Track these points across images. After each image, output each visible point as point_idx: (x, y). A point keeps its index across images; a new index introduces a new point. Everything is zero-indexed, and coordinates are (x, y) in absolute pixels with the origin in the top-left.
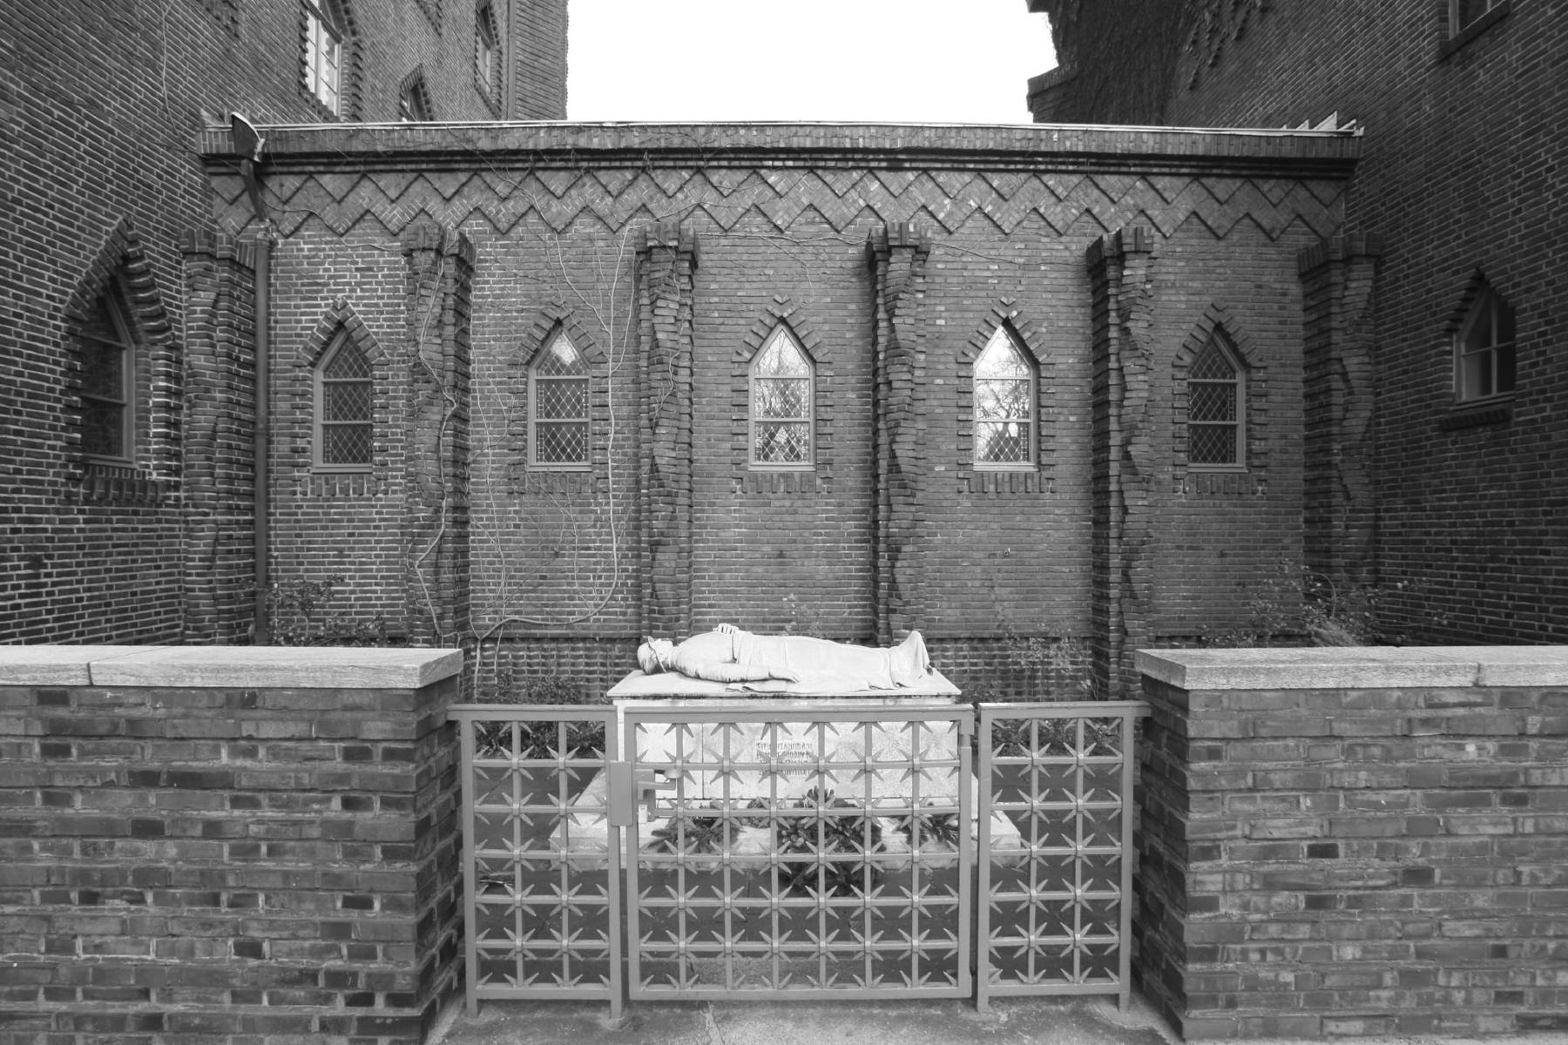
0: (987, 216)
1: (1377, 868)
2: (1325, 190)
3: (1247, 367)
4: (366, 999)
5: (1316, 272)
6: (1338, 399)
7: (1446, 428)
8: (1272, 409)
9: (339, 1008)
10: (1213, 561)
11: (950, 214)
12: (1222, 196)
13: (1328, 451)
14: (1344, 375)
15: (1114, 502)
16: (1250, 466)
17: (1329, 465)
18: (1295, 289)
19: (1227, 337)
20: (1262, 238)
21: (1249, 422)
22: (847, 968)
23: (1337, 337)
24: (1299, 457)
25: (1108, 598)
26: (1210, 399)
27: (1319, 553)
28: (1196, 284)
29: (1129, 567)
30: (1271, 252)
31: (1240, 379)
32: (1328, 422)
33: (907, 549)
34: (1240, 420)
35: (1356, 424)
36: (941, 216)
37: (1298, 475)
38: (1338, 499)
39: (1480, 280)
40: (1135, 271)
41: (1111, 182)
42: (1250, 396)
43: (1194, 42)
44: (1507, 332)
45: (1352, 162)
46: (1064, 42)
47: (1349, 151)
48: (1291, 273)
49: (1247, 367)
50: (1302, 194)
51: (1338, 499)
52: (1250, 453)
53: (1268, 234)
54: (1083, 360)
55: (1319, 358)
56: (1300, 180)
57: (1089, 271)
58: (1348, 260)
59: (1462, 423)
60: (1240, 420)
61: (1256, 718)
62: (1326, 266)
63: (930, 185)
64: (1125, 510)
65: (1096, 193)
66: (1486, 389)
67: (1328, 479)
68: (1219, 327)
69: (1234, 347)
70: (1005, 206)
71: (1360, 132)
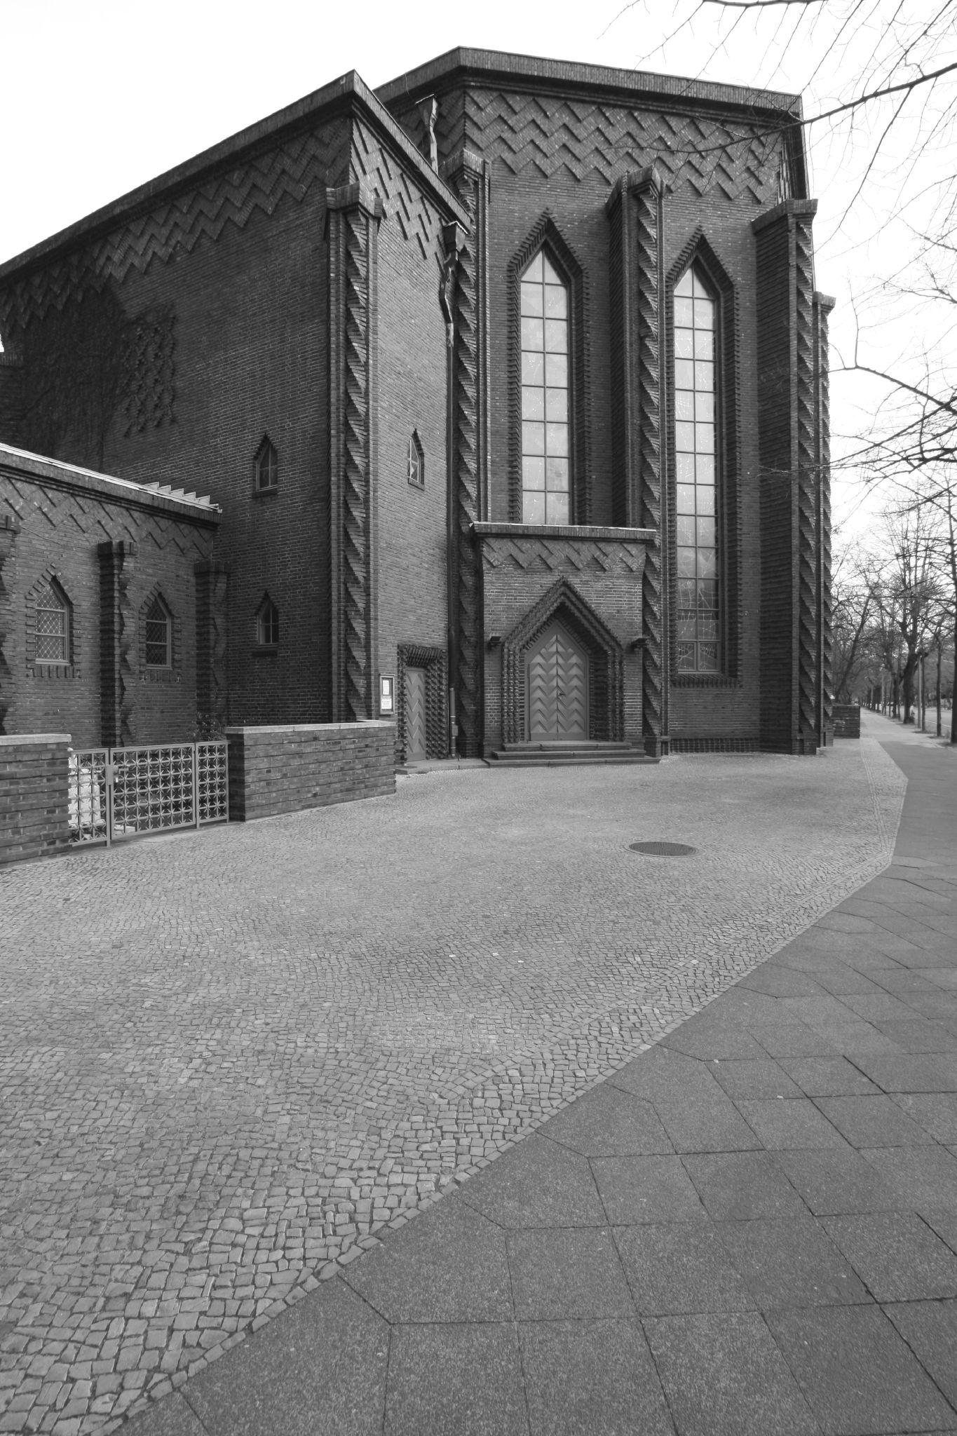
0: (44, 513)
1: (279, 775)
2: (206, 535)
3: (172, 616)
4: (53, 843)
5: (203, 573)
6: (212, 637)
7: (255, 655)
8: (181, 636)
9: (45, 847)
10: (158, 715)
11: (22, 508)
12: (163, 528)
13: (208, 662)
14: (215, 626)
15: (117, 684)
16: (174, 667)
17: (209, 668)
18: (193, 580)
19: (163, 600)
20: (178, 551)
21: (173, 644)
22: (167, 821)
23: (212, 608)
24: (194, 663)
25: (114, 735)
26: (153, 632)
27: (204, 706)
28: (150, 571)
29: (126, 718)
30: (183, 560)
31: (168, 621)
32: (208, 647)
33: (11, 710)
34: (168, 643)
35: (220, 650)
36: (17, 508)
37: (193, 672)
38: (213, 685)
39: (266, 596)
40: (129, 564)
41: (111, 508)
42: (174, 631)
43: (127, 409)
44: (276, 620)
45: (218, 524)
46: (10, 336)
47: (216, 520)
48: (191, 571)
49: (172, 616)
50: (196, 533)
51: (213, 685)
52: (173, 660)
53: (182, 550)
54: (94, 604)
55: (203, 617)
56: (196, 527)
57: (99, 556)
58: (217, 572)
59: (260, 654)
60: (168, 643)
61: (256, 741)
62: (207, 573)
63: (11, 487)
64: (123, 688)
65: (103, 513)
66: (267, 640)
67: (208, 675)
68: (160, 594)
69: (166, 605)
70: (55, 510)
71: (220, 511)
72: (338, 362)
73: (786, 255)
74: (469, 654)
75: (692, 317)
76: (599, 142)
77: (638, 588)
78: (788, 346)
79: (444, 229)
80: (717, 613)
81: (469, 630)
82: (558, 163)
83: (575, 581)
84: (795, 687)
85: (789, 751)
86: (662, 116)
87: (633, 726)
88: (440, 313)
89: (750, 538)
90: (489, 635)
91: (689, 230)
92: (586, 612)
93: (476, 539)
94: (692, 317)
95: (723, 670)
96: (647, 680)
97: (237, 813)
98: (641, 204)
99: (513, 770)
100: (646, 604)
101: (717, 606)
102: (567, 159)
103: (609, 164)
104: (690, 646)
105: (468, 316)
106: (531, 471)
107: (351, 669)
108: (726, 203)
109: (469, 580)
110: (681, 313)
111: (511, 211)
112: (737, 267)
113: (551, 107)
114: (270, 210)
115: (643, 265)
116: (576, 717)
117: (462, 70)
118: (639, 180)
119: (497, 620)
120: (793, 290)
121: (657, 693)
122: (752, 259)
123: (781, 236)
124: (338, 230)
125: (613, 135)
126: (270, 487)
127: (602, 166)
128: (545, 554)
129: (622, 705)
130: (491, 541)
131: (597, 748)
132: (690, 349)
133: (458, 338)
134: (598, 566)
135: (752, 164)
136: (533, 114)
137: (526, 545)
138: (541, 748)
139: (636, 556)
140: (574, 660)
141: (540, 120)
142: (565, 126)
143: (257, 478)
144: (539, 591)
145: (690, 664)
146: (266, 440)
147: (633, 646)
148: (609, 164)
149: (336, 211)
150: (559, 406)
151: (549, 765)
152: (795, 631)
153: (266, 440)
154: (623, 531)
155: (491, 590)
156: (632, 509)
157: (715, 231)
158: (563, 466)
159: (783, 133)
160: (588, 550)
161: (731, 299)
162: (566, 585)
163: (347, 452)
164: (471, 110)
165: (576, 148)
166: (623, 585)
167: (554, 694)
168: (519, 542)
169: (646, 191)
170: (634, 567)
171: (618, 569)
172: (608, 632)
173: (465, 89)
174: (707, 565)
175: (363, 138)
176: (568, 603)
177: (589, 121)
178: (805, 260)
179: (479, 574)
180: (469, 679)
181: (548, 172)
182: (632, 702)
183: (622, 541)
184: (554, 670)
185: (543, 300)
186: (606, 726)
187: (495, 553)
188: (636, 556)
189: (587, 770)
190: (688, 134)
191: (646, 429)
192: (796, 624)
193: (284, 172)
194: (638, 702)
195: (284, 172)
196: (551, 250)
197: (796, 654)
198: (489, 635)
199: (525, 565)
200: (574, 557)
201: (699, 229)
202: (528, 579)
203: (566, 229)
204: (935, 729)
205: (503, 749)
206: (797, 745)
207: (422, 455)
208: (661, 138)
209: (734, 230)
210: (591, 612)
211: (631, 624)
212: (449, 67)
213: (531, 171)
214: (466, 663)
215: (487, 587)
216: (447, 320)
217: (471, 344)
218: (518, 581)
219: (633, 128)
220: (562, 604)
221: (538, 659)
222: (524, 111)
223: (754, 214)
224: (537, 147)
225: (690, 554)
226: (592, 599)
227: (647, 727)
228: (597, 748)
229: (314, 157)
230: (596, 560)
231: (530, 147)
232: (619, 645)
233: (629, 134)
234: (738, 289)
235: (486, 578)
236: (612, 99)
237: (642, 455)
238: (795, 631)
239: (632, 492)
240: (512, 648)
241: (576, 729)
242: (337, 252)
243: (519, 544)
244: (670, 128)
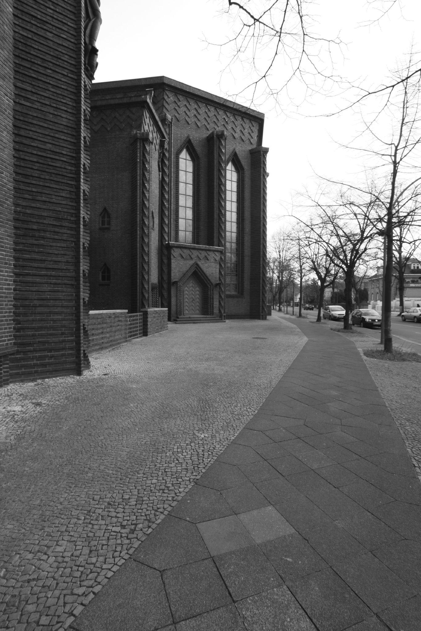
72: (140, 189)
73: (260, 163)
74: (165, 286)
75: (231, 176)
76: (206, 116)
77: (218, 266)
78: (260, 192)
79: (161, 141)
81: (165, 278)
82: (193, 120)
83: (199, 263)
84: (261, 299)
85: (259, 319)
86: (225, 112)
87: (216, 311)
88: (157, 168)
89: (247, 251)
91: (232, 149)
93: (169, 248)
94: (231, 176)
95: (239, 293)
96: (220, 296)
97: (145, 333)
98: (220, 142)
99: (183, 325)
100: (220, 272)
101: (237, 272)
102: (196, 119)
103: (209, 124)
104: (229, 285)
105: (166, 170)
106: (182, 222)
107: (144, 291)
108: (242, 143)
109: (165, 261)
110: (228, 176)
111: (179, 134)
112: (245, 163)
113: (192, 102)
114: (109, 129)
115: (220, 161)
116: (198, 308)
117: (164, 84)
118: (220, 134)
119: (176, 274)
120: (262, 175)
121: (222, 299)
122: (250, 161)
123: (258, 156)
124: (140, 146)
125: (210, 115)
126: (106, 226)
127: (206, 124)
128: (191, 254)
129: (213, 304)
130: (174, 249)
131: (206, 318)
132: (230, 187)
133: (163, 177)
134: (206, 258)
135: (250, 132)
136: (185, 103)
137: (185, 251)
138: (190, 318)
139: (218, 256)
140: (198, 289)
141: (188, 105)
142: (195, 109)
143: (101, 222)
144: (188, 266)
145: (229, 291)
146: (105, 209)
147: (217, 285)
148: (209, 124)
149: (140, 139)
150: (190, 203)
151: (194, 323)
152: (261, 281)
153: (105, 209)
154: (212, 247)
155: (174, 264)
156: (216, 240)
157: (239, 151)
158: (191, 222)
159: (259, 124)
160: (204, 254)
161: (243, 173)
162: (197, 264)
163: (143, 220)
164: (166, 97)
165: (199, 117)
166: (213, 265)
167: (191, 300)
168: (183, 250)
169: (222, 137)
170: (217, 259)
171: (212, 260)
172: (209, 280)
173: (164, 90)
174: (234, 259)
175: (146, 114)
177: (203, 109)
178: (265, 165)
179: (169, 260)
180: (165, 294)
181: (190, 123)
182: (216, 304)
183: (214, 251)
184: (190, 294)
185: (186, 164)
186: (208, 311)
187: (175, 253)
188: (218, 256)
189: (206, 324)
190: (232, 118)
191: (220, 215)
192: (261, 279)
193: (115, 117)
194: (218, 303)
195: (115, 117)
197: (261, 288)
200: (199, 255)
201: (234, 149)
202: (185, 262)
203: (195, 143)
204: (298, 314)
205: (178, 318)
206: (261, 317)
208: (224, 118)
209: (245, 151)
210: (204, 274)
211: (216, 278)
212: (159, 82)
213: (184, 122)
215: (172, 264)
216: (159, 171)
217: (167, 179)
218: (182, 262)
219: (216, 114)
221: (186, 288)
222: (183, 102)
223: (250, 148)
224: (186, 114)
225: (229, 255)
226: (205, 269)
227: (220, 311)
228: (206, 318)
229: (128, 117)
230: (206, 256)
231: (184, 113)
232: (212, 284)
233: (215, 115)
234: (245, 170)
235: (172, 261)
236: (210, 103)
237: (219, 222)
238: (261, 281)
239: (216, 235)
241: (198, 312)
242: (140, 153)
244: (227, 116)
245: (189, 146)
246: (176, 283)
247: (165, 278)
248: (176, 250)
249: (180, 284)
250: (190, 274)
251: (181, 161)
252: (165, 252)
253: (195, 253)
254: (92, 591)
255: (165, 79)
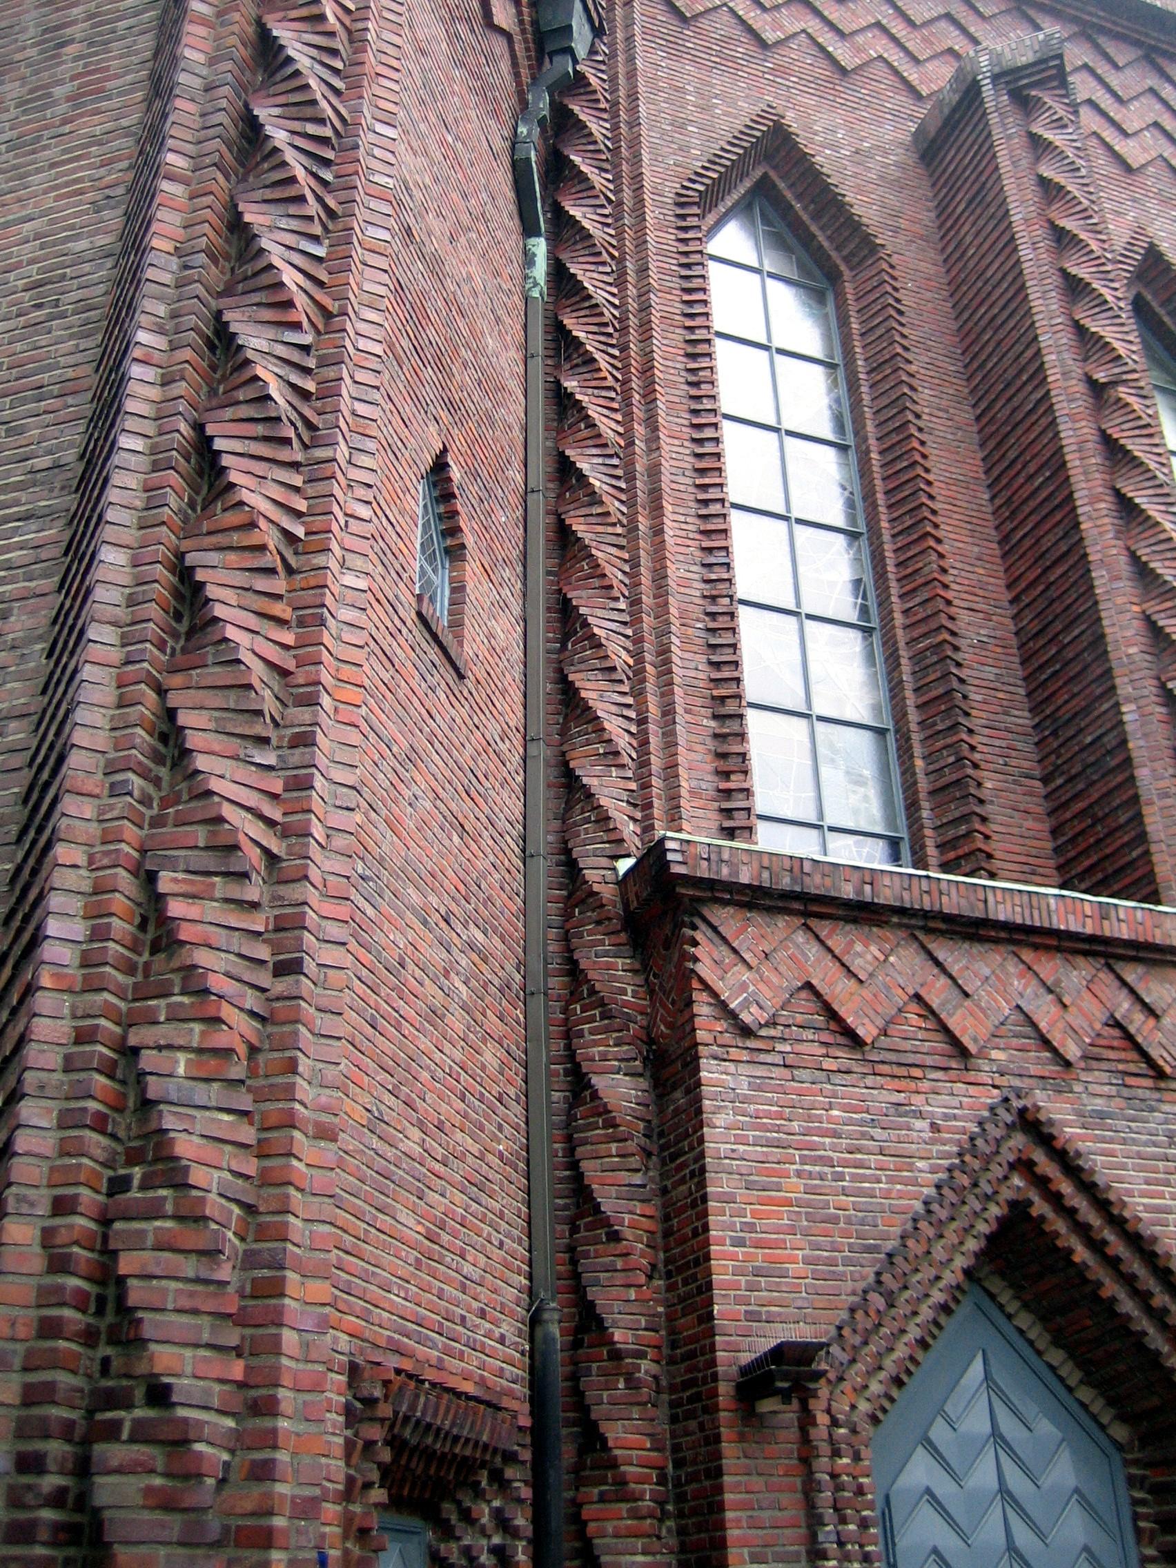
74: (631, 1436)
80: (101, 1301)
81: (629, 1315)
83: (1058, 1111)
90: (740, 1341)
92: (1117, 1247)
93: (663, 908)
109: (621, 1089)
119: (775, 1270)
128: (938, 993)
137: (864, 950)
162: (1032, 1125)
168: (840, 937)
176: (1040, 1207)
179: (671, 1068)
187: (744, 969)
196: (784, 210)
198: (740, 1341)
199: (866, 1031)
201: (1140, 230)
207: (455, 553)
214: (622, 1492)
216: (529, 229)
218: (843, 1102)
220: (1019, 1208)
221: (921, 1471)
240: (841, 1407)
243: (837, 942)
245: (777, 186)
246: (788, 1372)
247: (629, 1315)
248: (752, 933)
249: (842, 1400)
250: (957, 1254)
251: (719, 279)
252: (613, 970)
253: (992, 989)
254: (804, 31)
255: (572, 121)
